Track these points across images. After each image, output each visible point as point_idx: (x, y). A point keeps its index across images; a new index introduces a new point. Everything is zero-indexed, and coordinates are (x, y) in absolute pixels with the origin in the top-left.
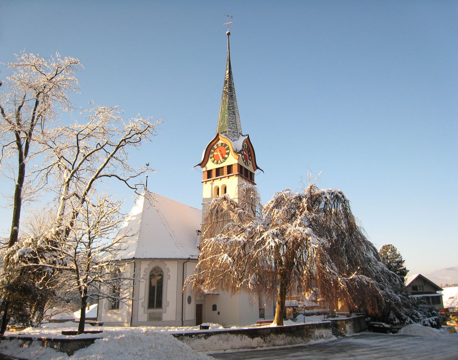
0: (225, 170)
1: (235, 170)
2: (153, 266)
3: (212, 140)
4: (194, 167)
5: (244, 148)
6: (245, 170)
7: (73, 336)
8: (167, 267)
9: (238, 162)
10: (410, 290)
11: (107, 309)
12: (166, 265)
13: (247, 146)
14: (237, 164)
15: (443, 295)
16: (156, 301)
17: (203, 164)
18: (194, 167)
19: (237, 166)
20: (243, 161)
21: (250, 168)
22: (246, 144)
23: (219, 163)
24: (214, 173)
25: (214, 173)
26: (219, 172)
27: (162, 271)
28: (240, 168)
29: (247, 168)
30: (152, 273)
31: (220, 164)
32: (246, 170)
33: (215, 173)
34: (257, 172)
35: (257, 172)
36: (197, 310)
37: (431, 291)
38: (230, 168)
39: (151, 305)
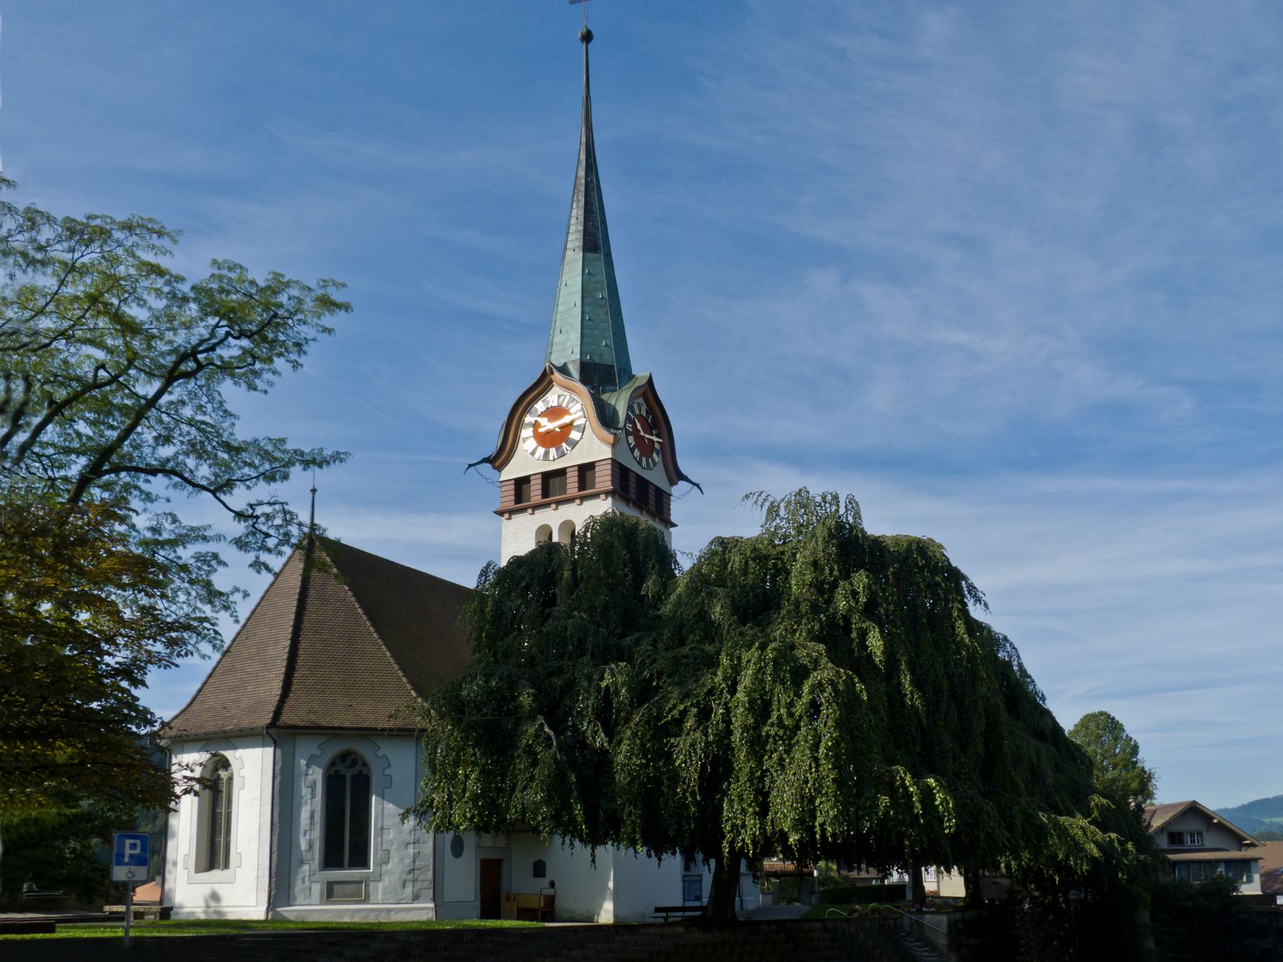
0: (572, 479)
1: (604, 478)
2: (334, 749)
3: (585, 77)
4: (470, 466)
5: (633, 412)
6: (636, 480)
7: (655, 404)
8: (380, 753)
9: (613, 453)
10: (1163, 843)
11: (192, 867)
12: (380, 748)
13: (644, 408)
14: (610, 461)
15: (304, 469)
16: (350, 845)
17: (499, 458)
18: (470, 466)
19: (609, 467)
20: (633, 453)
21: (656, 476)
22: (641, 400)
23: (551, 458)
24: (535, 489)
25: (535, 489)
26: (551, 480)
27: (365, 764)
28: (620, 471)
29: (646, 475)
30: (335, 768)
31: (554, 460)
32: (643, 483)
33: (540, 487)
34: (678, 490)
35: (679, 489)
36: (482, 874)
37: (1223, 847)
38: (586, 471)
39: (332, 858)
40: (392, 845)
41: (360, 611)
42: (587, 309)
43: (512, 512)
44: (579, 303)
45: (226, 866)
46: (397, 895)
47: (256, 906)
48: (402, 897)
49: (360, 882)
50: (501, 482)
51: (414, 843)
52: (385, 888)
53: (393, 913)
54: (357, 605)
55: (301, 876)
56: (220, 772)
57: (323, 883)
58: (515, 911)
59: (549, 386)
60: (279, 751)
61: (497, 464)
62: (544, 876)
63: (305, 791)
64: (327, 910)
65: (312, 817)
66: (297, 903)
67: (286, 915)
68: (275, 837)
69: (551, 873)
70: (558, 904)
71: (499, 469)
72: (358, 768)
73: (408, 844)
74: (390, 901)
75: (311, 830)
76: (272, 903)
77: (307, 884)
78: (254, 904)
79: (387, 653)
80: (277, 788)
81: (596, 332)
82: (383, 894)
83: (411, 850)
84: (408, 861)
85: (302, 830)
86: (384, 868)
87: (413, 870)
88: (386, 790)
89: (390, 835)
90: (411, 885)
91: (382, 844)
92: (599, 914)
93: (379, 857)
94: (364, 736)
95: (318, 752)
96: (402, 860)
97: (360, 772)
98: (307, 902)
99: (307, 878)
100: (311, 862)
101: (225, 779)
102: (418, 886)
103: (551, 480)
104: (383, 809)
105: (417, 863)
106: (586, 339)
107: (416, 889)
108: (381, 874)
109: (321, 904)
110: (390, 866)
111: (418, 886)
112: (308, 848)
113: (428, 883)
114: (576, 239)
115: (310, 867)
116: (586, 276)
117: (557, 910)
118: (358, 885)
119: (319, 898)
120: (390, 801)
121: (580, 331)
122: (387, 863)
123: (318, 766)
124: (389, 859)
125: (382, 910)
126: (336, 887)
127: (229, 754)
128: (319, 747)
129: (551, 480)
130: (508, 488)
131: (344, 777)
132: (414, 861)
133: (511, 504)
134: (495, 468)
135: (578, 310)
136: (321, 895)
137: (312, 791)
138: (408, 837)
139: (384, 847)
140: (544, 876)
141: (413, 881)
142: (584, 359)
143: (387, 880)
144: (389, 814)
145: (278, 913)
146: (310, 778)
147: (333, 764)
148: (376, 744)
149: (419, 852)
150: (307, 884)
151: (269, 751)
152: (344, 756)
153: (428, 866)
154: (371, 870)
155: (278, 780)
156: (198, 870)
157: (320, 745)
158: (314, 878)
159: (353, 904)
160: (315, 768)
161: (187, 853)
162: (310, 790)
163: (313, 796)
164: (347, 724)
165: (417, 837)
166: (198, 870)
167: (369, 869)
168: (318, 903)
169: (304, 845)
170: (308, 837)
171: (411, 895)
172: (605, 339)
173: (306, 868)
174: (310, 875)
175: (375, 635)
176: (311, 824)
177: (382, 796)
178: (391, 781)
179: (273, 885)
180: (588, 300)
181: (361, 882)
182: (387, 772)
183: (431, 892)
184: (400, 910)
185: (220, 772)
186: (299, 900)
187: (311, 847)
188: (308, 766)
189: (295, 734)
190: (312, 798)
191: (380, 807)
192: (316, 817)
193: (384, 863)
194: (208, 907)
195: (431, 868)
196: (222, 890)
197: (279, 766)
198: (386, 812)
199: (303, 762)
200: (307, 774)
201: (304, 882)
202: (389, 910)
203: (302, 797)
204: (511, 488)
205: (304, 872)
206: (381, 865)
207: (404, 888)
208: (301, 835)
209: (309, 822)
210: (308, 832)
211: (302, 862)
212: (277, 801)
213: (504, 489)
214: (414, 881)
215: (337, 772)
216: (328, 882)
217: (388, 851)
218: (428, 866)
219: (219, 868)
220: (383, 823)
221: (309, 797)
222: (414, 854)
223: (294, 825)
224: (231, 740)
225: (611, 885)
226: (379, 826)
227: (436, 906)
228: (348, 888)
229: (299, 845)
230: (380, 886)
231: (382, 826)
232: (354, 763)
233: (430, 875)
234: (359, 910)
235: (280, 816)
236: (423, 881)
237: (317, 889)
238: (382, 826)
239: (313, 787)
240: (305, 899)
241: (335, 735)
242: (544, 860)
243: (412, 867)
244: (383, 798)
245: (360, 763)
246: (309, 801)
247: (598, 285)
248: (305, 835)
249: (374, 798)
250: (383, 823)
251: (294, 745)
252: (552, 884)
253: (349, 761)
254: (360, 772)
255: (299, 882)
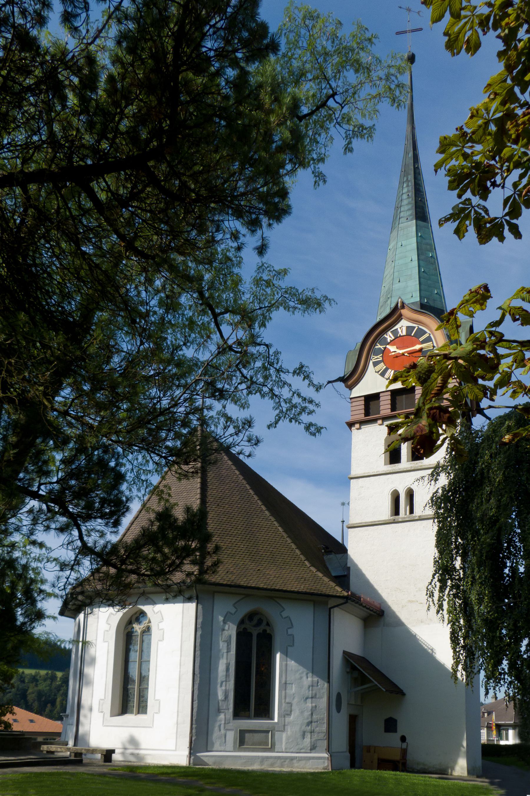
2: (246, 609)
8: (284, 614)
12: (284, 609)
18: (329, 382)
27: (268, 624)
40: (293, 699)
41: (251, 491)
42: (422, 263)
43: (362, 423)
44: (415, 258)
45: (142, 709)
46: (298, 744)
47: (175, 750)
48: (301, 747)
49: (267, 732)
50: (351, 399)
51: (312, 698)
52: (288, 738)
53: (295, 761)
54: (248, 487)
55: (218, 724)
56: (134, 625)
57: (236, 732)
58: (376, 762)
59: (400, 318)
60: (200, 607)
61: (349, 383)
62: (395, 731)
63: (223, 646)
64: (240, 756)
65: (227, 669)
66: (215, 749)
67: (206, 760)
68: (196, 687)
69: (402, 730)
70: (409, 757)
71: (351, 388)
72: (263, 627)
73: (307, 698)
74: (291, 750)
75: (226, 681)
76: (193, 749)
77: (223, 731)
78: (174, 749)
79: (279, 528)
80: (198, 641)
81: (429, 282)
82: (286, 743)
83: (309, 705)
84: (307, 714)
85: (219, 681)
86: (287, 719)
87: (311, 722)
88: (289, 648)
89: (293, 690)
90: (309, 736)
91: (285, 698)
92: (453, 769)
93: (283, 709)
94: (271, 598)
95: (233, 610)
96: (302, 712)
97: (265, 631)
98: (222, 748)
99: (222, 726)
100: (226, 711)
101: (139, 631)
102: (315, 737)
103: (398, 398)
104: (286, 665)
105: (314, 716)
106: (422, 286)
107: (313, 740)
108: (284, 725)
109: (234, 751)
110: (292, 718)
111: (315, 737)
112: (223, 698)
113: (323, 734)
114: (409, 210)
115: (225, 715)
116: (419, 238)
117: (408, 762)
118: (265, 734)
119: (232, 745)
120: (292, 659)
121: (418, 279)
122: (289, 715)
123: (233, 623)
124: (291, 711)
125: (286, 758)
126: (247, 735)
127: (147, 608)
128: (234, 605)
129: (398, 398)
130: (358, 403)
131: (250, 635)
132: (312, 714)
133: (362, 417)
134: (347, 386)
135: (415, 263)
136: (235, 743)
137: (228, 646)
138: (307, 692)
139: (287, 700)
140: (395, 731)
141: (311, 732)
142: (422, 302)
143: (289, 730)
144: (292, 670)
145: (198, 757)
146: (226, 633)
147: (242, 622)
148: (280, 605)
149: (316, 706)
150: (223, 731)
151: (191, 607)
152: (251, 616)
153: (323, 719)
154: (276, 720)
155: (199, 633)
156: (112, 715)
157: (236, 603)
158: (228, 726)
159: (264, 752)
160: (231, 624)
161: (103, 698)
162: (226, 645)
163: (228, 651)
164: (261, 586)
165: (314, 692)
166: (112, 715)
167: (273, 719)
168: (232, 749)
169: (220, 696)
170: (224, 688)
171: (309, 745)
172: (436, 288)
173: (222, 716)
174: (225, 723)
175: (267, 512)
176: (226, 675)
177: (286, 653)
178: (293, 640)
179: (194, 731)
180: (422, 257)
181: (267, 732)
182: (290, 631)
183: (325, 743)
184: (301, 759)
185: (134, 625)
186: (217, 746)
187: (226, 697)
188: (225, 622)
189: (214, 592)
190: (227, 652)
191: (284, 663)
192: (230, 671)
193: (288, 715)
194: (125, 749)
195: (325, 721)
196: (141, 735)
197: (200, 621)
198: (289, 669)
199: (221, 618)
200: (223, 630)
201: (220, 730)
202: (292, 759)
203: (219, 651)
204: (361, 405)
205: (220, 721)
206: (284, 717)
207: (304, 738)
208: (219, 685)
209: (225, 673)
210: (224, 683)
211: (219, 711)
212: (198, 653)
213: (354, 404)
214: (312, 732)
215: (245, 629)
216: (240, 730)
217: (290, 704)
218: (323, 719)
219: (132, 713)
220: (286, 678)
221: (225, 651)
222: (312, 707)
223: (212, 676)
224: (150, 596)
225: (465, 744)
226: (283, 682)
227: (331, 756)
228: (257, 737)
229: (216, 694)
230: (284, 735)
231: (286, 681)
232: (260, 622)
233: (324, 728)
234: (268, 758)
235: (200, 667)
236: (319, 733)
237: (231, 736)
238: (286, 681)
239: (228, 642)
240: (220, 746)
241: (247, 596)
242: (395, 717)
243: (310, 720)
244: (287, 656)
245: (264, 623)
246: (225, 655)
247: (428, 247)
248: (221, 686)
249: (278, 656)
250: (286, 678)
251: (213, 601)
252: (403, 739)
253: (255, 621)
254: (265, 631)
255: (216, 728)
